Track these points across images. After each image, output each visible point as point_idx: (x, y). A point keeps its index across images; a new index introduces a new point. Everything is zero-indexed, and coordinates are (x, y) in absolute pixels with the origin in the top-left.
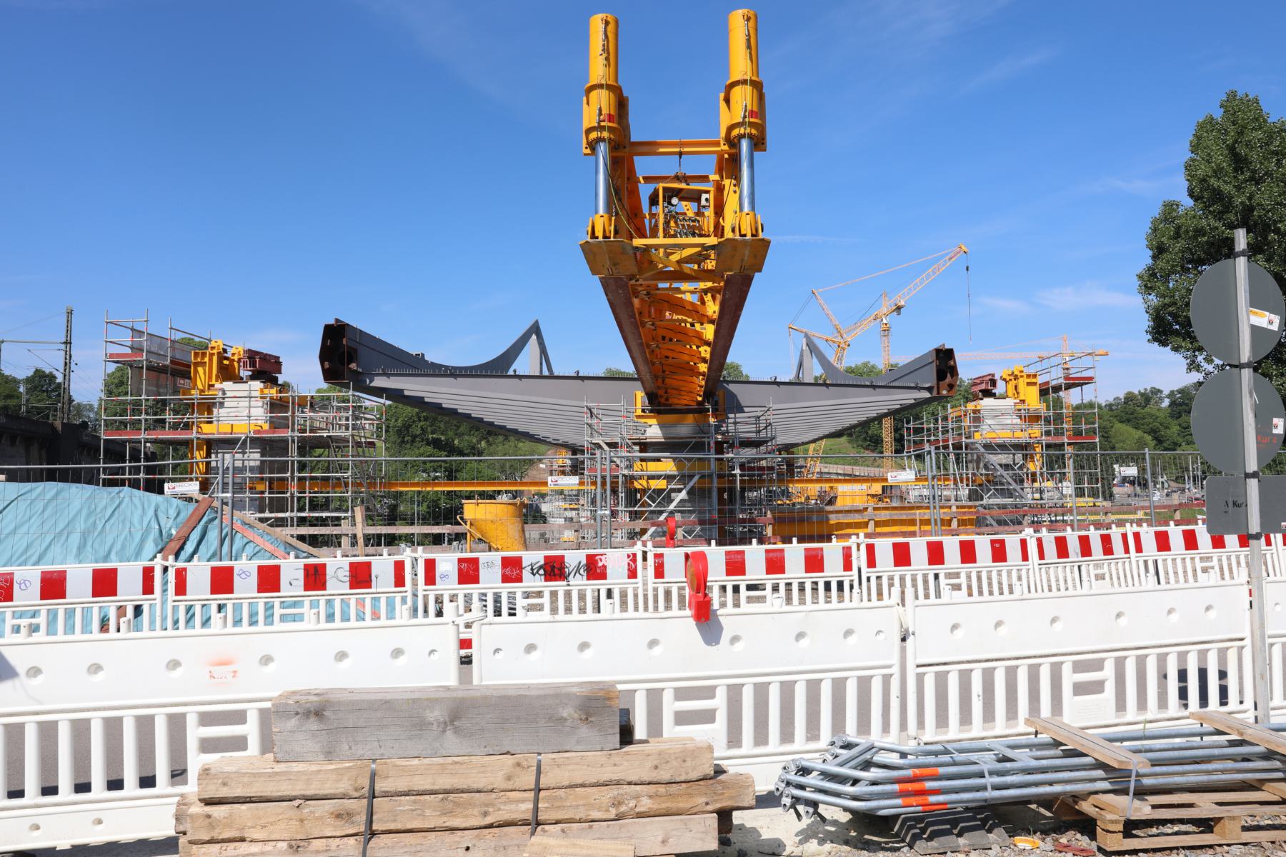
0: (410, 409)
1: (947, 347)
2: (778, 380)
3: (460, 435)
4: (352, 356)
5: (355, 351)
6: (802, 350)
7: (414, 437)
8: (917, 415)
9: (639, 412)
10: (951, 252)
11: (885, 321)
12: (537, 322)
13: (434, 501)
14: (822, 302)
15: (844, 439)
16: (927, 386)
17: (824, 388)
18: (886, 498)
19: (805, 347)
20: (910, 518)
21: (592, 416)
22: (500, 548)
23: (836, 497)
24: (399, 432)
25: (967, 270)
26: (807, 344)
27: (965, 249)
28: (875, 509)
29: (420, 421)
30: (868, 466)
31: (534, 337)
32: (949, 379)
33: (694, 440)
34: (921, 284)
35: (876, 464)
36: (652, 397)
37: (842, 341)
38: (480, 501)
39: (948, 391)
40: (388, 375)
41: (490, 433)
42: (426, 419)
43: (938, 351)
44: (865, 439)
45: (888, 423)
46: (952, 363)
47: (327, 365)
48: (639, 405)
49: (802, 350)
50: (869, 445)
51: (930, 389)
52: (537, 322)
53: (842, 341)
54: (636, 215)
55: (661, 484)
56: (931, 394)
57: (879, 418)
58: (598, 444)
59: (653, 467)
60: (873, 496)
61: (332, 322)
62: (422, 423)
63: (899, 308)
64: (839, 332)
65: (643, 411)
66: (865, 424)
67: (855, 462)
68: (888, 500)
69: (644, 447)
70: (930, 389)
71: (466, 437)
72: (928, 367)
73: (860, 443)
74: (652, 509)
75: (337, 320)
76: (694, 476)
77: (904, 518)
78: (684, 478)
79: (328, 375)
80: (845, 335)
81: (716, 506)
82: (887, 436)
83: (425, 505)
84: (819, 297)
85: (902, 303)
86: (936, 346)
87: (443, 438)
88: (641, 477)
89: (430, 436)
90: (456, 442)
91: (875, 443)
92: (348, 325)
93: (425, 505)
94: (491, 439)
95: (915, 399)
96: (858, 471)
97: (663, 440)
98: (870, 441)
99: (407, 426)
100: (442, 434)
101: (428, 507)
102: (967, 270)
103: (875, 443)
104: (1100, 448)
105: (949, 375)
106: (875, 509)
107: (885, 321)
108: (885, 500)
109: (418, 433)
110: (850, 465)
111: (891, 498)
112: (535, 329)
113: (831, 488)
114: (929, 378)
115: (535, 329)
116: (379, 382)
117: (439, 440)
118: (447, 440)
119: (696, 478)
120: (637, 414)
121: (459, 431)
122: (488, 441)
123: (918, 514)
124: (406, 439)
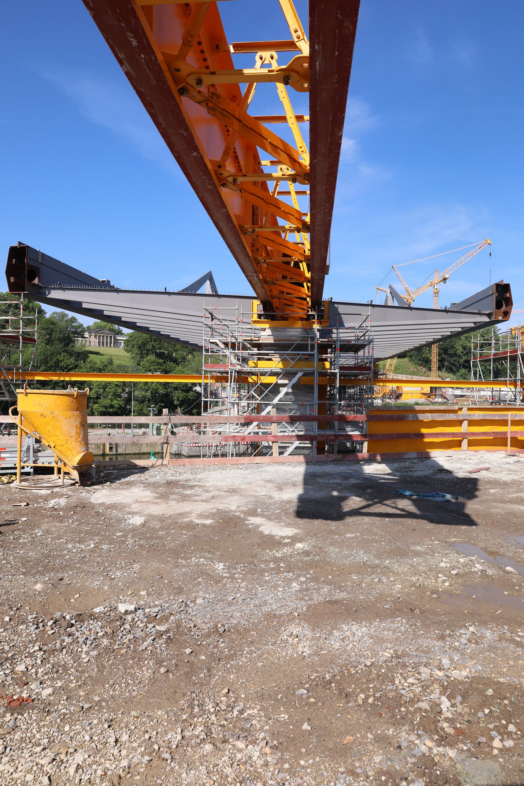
0: (146, 335)
1: (505, 282)
2: (373, 303)
3: (176, 351)
4: (33, 273)
5: (38, 269)
6: (387, 296)
7: (148, 350)
8: (453, 346)
9: (255, 318)
10: (480, 244)
11: (436, 287)
12: (210, 272)
13: (156, 390)
14: (398, 273)
15: (406, 359)
16: (487, 312)
17: (409, 311)
18: (432, 395)
19: (389, 294)
20: (502, 418)
21: (212, 319)
22: (52, 445)
23: (402, 394)
24: (139, 348)
25: (490, 255)
26: (391, 293)
27: (489, 242)
28: (469, 409)
29: (152, 341)
30: (421, 376)
31: (208, 282)
32: (504, 308)
33: (296, 343)
34: (453, 269)
35: (426, 375)
36: (267, 305)
37: (410, 298)
38: (29, 391)
39: (503, 317)
40: (64, 289)
41: (194, 350)
42: (155, 341)
43: (498, 286)
44: (420, 360)
45: (435, 349)
46: (508, 295)
47: (12, 279)
48: (255, 311)
49: (387, 296)
50: (422, 363)
51: (489, 315)
52: (210, 272)
53: (410, 298)
54: (217, 47)
55: (272, 380)
56: (490, 319)
57: (429, 345)
58: (216, 342)
59: (264, 365)
60: (424, 394)
61: (16, 244)
62: (153, 343)
63: (445, 279)
64: (408, 292)
65: (260, 316)
66: (419, 349)
67: (413, 374)
68: (434, 397)
69: (259, 346)
70: (489, 315)
71: (180, 352)
72: (490, 297)
73: (417, 362)
74: (257, 402)
75: (20, 243)
76: (295, 374)
77: (497, 418)
78: (288, 374)
79: (12, 287)
80: (412, 295)
81: (316, 401)
82: (434, 358)
83: (149, 392)
84: (396, 270)
85: (447, 276)
86: (497, 281)
87: (166, 352)
88: (253, 374)
89: (158, 351)
90: (174, 355)
91: (426, 362)
92: (28, 247)
93: (149, 392)
94: (194, 353)
95: (474, 323)
96: (415, 378)
97: (273, 342)
98: (423, 361)
99: (144, 344)
100: (166, 350)
101: (152, 393)
102: (490, 255)
103: (426, 362)
104: (258, 395)
105: (504, 305)
106: (469, 409)
107: (436, 287)
108: (432, 397)
109: (150, 348)
110: (410, 375)
111: (435, 395)
112: (209, 277)
113: (398, 387)
114: (490, 306)
115: (209, 277)
116: (55, 294)
117: (164, 353)
118: (169, 353)
119: (299, 375)
120: (254, 319)
121: (175, 348)
122: (193, 355)
123: (510, 415)
124: (143, 352)
